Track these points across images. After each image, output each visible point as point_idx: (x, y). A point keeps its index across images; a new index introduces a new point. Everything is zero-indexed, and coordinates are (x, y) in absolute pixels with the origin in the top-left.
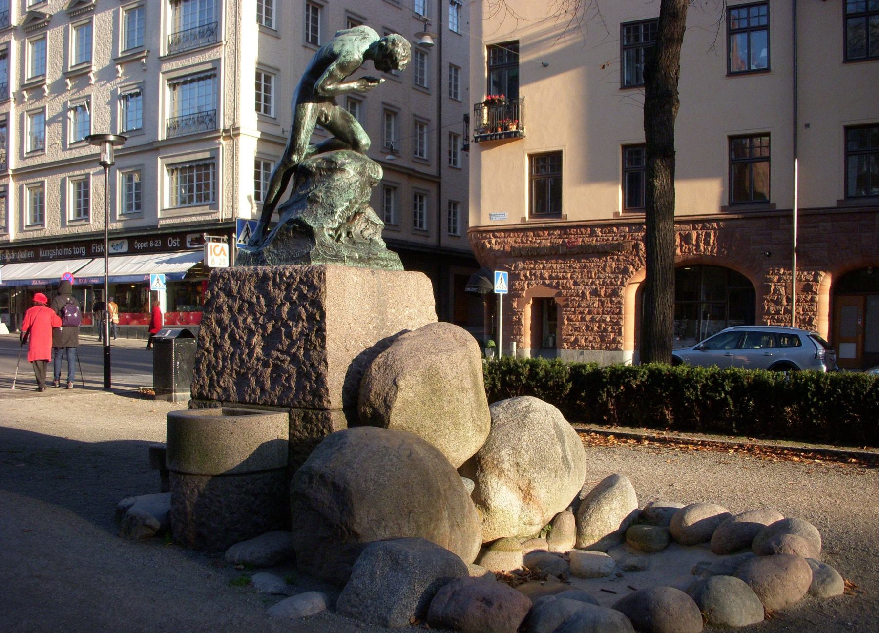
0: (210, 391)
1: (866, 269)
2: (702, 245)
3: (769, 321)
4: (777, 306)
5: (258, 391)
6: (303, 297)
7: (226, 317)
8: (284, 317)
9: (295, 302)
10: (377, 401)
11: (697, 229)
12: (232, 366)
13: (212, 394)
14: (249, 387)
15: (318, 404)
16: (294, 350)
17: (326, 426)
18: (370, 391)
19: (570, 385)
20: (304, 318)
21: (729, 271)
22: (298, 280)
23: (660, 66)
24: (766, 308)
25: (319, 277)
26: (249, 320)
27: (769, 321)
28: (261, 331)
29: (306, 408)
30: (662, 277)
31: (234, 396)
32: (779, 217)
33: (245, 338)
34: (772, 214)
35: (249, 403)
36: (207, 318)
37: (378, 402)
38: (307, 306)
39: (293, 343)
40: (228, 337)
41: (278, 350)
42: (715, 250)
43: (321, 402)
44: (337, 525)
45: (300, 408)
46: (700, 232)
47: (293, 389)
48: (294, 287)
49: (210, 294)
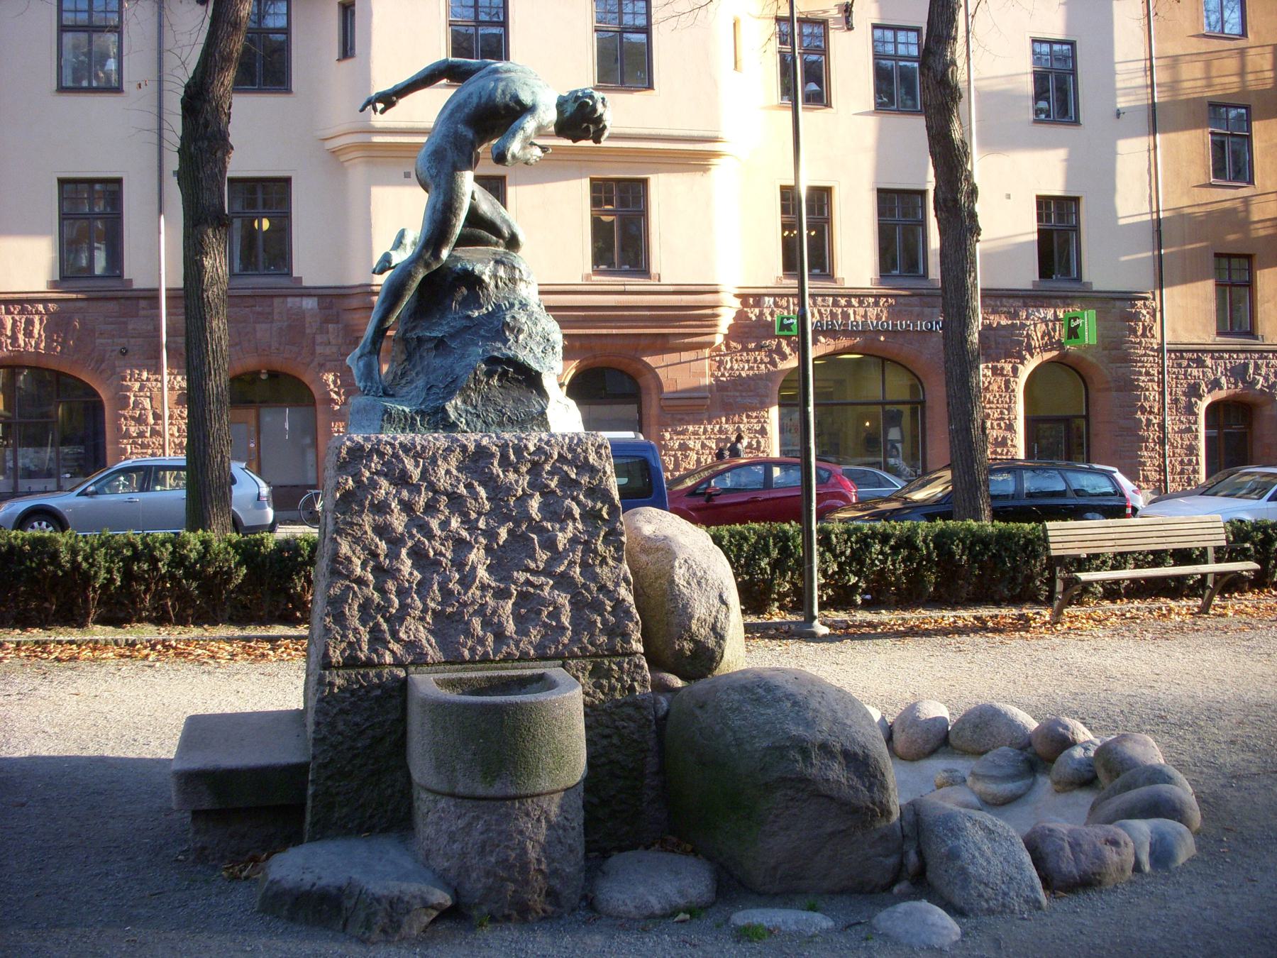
0: (372, 649)
1: (259, 372)
2: (21, 337)
3: (129, 447)
4: (140, 425)
5: (490, 638)
6: (567, 482)
7: (398, 521)
8: (534, 515)
9: (553, 492)
10: (702, 631)
11: (12, 313)
12: (425, 604)
13: (380, 656)
14: (468, 633)
15: (622, 646)
16: (562, 568)
17: (638, 678)
18: (691, 617)
19: (244, 570)
20: (577, 516)
21: (58, 375)
22: (556, 457)
23: (211, 95)
24: (124, 428)
25: (597, 453)
26: (455, 523)
27: (129, 447)
28: (483, 540)
29: (596, 655)
30: (217, 400)
31: (433, 653)
32: (138, 298)
33: (449, 555)
34: (129, 294)
35: (472, 661)
36: (351, 524)
37: (703, 633)
38: (581, 497)
39: (557, 556)
40: (408, 554)
41: (527, 570)
42: (43, 345)
43: (629, 642)
44: (868, 808)
45: (584, 657)
46: (17, 318)
47: (564, 628)
48: (548, 467)
49: (350, 482)
